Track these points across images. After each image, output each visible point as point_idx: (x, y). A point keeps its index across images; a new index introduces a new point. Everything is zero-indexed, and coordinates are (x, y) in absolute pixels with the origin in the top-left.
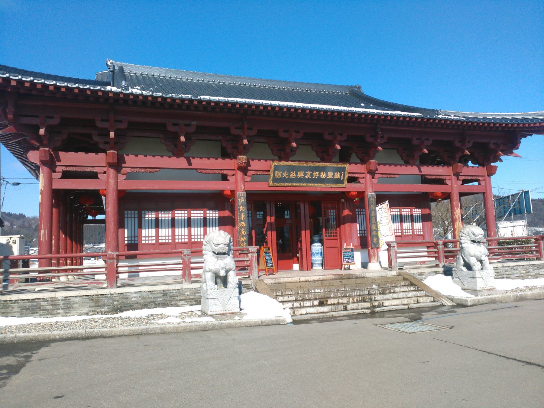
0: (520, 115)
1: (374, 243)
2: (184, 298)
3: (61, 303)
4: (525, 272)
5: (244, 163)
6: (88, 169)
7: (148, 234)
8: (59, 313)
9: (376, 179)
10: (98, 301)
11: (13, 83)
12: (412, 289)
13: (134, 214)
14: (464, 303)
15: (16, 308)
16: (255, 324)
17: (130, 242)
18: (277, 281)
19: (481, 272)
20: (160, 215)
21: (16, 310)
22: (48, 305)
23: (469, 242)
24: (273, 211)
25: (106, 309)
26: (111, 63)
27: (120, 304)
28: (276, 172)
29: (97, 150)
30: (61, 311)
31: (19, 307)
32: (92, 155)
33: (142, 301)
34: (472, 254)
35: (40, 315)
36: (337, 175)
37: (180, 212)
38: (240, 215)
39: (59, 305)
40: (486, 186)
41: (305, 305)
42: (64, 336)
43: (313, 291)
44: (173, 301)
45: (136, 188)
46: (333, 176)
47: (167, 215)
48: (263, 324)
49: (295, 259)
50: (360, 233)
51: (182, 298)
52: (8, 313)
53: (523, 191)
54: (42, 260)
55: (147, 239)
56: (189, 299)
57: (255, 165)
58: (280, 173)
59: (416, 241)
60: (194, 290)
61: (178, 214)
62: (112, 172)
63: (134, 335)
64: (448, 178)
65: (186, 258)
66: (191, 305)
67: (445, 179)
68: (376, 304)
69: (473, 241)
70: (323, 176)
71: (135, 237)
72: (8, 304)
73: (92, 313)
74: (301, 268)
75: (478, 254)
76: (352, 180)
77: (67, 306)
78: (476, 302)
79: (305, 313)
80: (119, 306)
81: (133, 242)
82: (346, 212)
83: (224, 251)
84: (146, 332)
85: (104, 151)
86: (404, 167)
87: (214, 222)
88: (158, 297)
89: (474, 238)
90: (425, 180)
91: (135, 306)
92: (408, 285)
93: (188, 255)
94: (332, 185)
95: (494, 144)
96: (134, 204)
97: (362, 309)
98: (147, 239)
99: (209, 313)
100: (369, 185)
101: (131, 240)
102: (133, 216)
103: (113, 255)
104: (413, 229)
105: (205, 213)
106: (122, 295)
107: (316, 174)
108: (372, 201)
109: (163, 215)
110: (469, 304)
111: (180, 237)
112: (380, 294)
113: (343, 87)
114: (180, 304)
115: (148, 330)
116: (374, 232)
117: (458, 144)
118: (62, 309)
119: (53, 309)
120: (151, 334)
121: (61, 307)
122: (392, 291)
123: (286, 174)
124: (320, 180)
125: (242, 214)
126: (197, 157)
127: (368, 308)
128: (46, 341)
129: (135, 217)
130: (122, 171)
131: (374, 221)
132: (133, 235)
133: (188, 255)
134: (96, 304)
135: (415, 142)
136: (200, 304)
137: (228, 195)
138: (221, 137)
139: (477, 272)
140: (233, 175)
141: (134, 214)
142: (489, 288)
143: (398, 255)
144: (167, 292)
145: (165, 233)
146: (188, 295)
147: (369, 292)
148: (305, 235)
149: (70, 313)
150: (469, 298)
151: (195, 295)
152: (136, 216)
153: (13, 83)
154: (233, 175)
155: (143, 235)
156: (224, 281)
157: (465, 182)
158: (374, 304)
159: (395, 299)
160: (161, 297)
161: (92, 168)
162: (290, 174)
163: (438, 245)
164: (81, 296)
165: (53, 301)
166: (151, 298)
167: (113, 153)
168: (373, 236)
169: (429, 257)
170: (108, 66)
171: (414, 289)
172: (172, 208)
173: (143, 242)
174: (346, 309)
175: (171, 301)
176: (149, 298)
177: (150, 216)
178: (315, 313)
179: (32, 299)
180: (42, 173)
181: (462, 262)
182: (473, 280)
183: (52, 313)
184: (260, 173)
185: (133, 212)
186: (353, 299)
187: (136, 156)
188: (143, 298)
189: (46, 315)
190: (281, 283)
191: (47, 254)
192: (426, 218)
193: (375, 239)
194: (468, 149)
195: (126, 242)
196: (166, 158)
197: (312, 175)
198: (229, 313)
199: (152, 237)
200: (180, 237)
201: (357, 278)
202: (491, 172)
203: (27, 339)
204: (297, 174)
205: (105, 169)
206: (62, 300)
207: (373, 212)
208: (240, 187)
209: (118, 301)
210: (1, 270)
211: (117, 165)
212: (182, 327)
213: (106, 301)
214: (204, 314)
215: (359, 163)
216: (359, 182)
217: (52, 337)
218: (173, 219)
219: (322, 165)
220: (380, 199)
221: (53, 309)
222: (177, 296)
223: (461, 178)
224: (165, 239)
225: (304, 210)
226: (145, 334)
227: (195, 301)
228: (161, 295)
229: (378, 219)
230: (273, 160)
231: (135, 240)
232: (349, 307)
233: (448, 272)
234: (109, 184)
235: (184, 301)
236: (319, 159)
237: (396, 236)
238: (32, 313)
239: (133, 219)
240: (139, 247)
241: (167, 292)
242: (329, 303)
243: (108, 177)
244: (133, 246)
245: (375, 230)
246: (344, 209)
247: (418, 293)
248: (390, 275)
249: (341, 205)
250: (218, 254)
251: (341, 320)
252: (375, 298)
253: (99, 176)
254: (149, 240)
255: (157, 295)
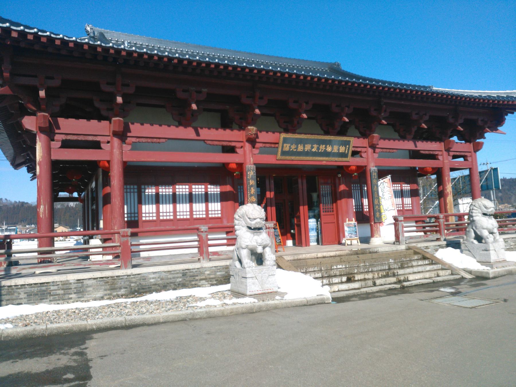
0: (505, 93)
1: (377, 218)
2: (204, 277)
3: (73, 286)
4: (514, 244)
5: (255, 134)
6: (90, 138)
7: (148, 211)
8: (71, 298)
9: (377, 153)
10: (113, 284)
11: (14, 35)
12: (427, 262)
13: (134, 189)
14: (484, 275)
15: (22, 294)
16: (301, 304)
17: (129, 219)
18: (296, 258)
19: (494, 244)
20: (160, 190)
21: (22, 296)
22: (59, 290)
23: (480, 215)
24: (273, 186)
25: (123, 291)
26: (91, 29)
27: (138, 286)
28: (285, 145)
29: (100, 118)
30: (73, 296)
31: (25, 293)
32: (94, 122)
33: (161, 282)
34: (485, 227)
35: (50, 301)
36: (342, 149)
37: (181, 187)
38: (250, 189)
39: (71, 289)
40: (472, 162)
41: (334, 282)
42: (102, 326)
43: (335, 267)
44: (193, 281)
45: (143, 160)
46: (339, 150)
47: (167, 190)
48: (309, 303)
49: (289, 235)
50: (355, 209)
51: (202, 278)
52: (13, 300)
53: (491, 168)
54: (42, 239)
55: (147, 215)
56: (210, 278)
57: (264, 137)
58: (288, 145)
59: (180, 228)
60: (214, 268)
61: (195, 188)
62: (116, 141)
63: (179, 321)
64: (440, 153)
65: (204, 235)
66: (212, 285)
67: (437, 155)
68: (402, 278)
69: (485, 214)
70: (329, 149)
71: (134, 213)
72: (12, 289)
73: (108, 297)
74: (294, 244)
75: (490, 227)
76: (355, 153)
77: (80, 291)
78: (497, 275)
79: (337, 290)
80: (137, 289)
81: (133, 219)
82: (342, 187)
83: (260, 226)
84: (190, 317)
85: (108, 119)
86: (401, 142)
87: (216, 198)
88: (177, 278)
89: (485, 211)
90: (415, 155)
91: (153, 287)
92: (420, 259)
93: (206, 232)
94: (336, 159)
95: (482, 121)
96: (140, 176)
97: (389, 284)
98: (147, 215)
99: (248, 293)
100: (370, 160)
101: (131, 217)
102: (132, 190)
103: (127, 232)
104: (403, 204)
105: (206, 188)
106: (139, 276)
107: (322, 147)
108: (375, 176)
109: (164, 190)
110: (491, 276)
111: (182, 214)
112: (399, 268)
113: (323, 63)
114: (200, 284)
115: (193, 314)
116: (377, 207)
117: (451, 120)
118: (75, 293)
119: (64, 294)
120: (197, 319)
121: (61, 291)
122: (410, 265)
123: (294, 147)
124: (326, 154)
125: (252, 188)
126: (205, 128)
127: (395, 283)
128: (82, 332)
129: (134, 192)
130: (127, 141)
131: (376, 196)
132: (133, 211)
133: (206, 232)
134: (112, 287)
135: (415, 117)
136: (229, 282)
137: (233, 169)
138: (228, 107)
139: (490, 244)
140: (242, 147)
141: (134, 189)
142: (501, 260)
143: (405, 229)
144: (187, 271)
145: (166, 209)
146: (208, 274)
147: (389, 266)
148: (303, 209)
149: (83, 297)
150: (491, 272)
151: (215, 274)
152: (136, 190)
153: (14, 35)
154: (242, 147)
155: (143, 211)
156: (259, 259)
157: (455, 157)
158: (400, 279)
159: (415, 273)
160: (180, 277)
161: (95, 137)
162: (297, 147)
163: (439, 219)
164: (94, 279)
165: (64, 284)
166: (171, 279)
167: (119, 120)
168: (376, 210)
169: (417, 232)
170: (87, 31)
171: (429, 262)
172: (172, 183)
173: (144, 219)
174: (375, 284)
175: (190, 281)
176: (168, 279)
177: (150, 191)
178: (346, 290)
179: (40, 283)
180: (40, 141)
181: (473, 235)
182: (485, 252)
183: (63, 298)
184: (267, 145)
185: (132, 187)
186: (378, 274)
187: (142, 124)
188: (162, 279)
189: (56, 300)
190: (300, 259)
191: (46, 233)
192: (414, 193)
193: (378, 214)
194: (460, 125)
195: (126, 219)
196: (173, 128)
197: (318, 148)
198: (268, 293)
199: (152, 213)
200: (198, 213)
201: (370, 253)
202: (478, 147)
203: (61, 330)
204: (304, 147)
205: (109, 139)
206: (74, 283)
207: (375, 187)
208: (249, 159)
209: (135, 283)
210: (2, 251)
211: (122, 135)
212: (228, 309)
213: (123, 283)
214: (237, 294)
215: (361, 137)
216: (361, 157)
217: (88, 328)
218: (174, 194)
219: (329, 139)
220: (382, 174)
221: (64, 294)
222: (197, 276)
223: (452, 154)
224: (166, 216)
225: (302, 185)
226: (190, 319)
227: (216, 280)
228: (181, 275)
229: (380, 194)
230: (280, 133)
231: (135, 217)
232: (378, 282)
233: (456, 245)
234: (115, 154)
235: (204, 281)
236: (322, 132)
237: (398, 211)
238: (41, 299)
239: (132, 194)
240: (140, 224)
241: (187, 271)
242: (356, 279)
243: (112, 147)
244: (133, 223)
245: (377, 205)
246: (340, 184)
247: (435, 267)
248: (400, 249)
249: (337, 181)
250: (255, 229)
251: (377, 297)
252: (397, 272)
253: (102, 145)
254: (149, 217)
255: (176, 275)
